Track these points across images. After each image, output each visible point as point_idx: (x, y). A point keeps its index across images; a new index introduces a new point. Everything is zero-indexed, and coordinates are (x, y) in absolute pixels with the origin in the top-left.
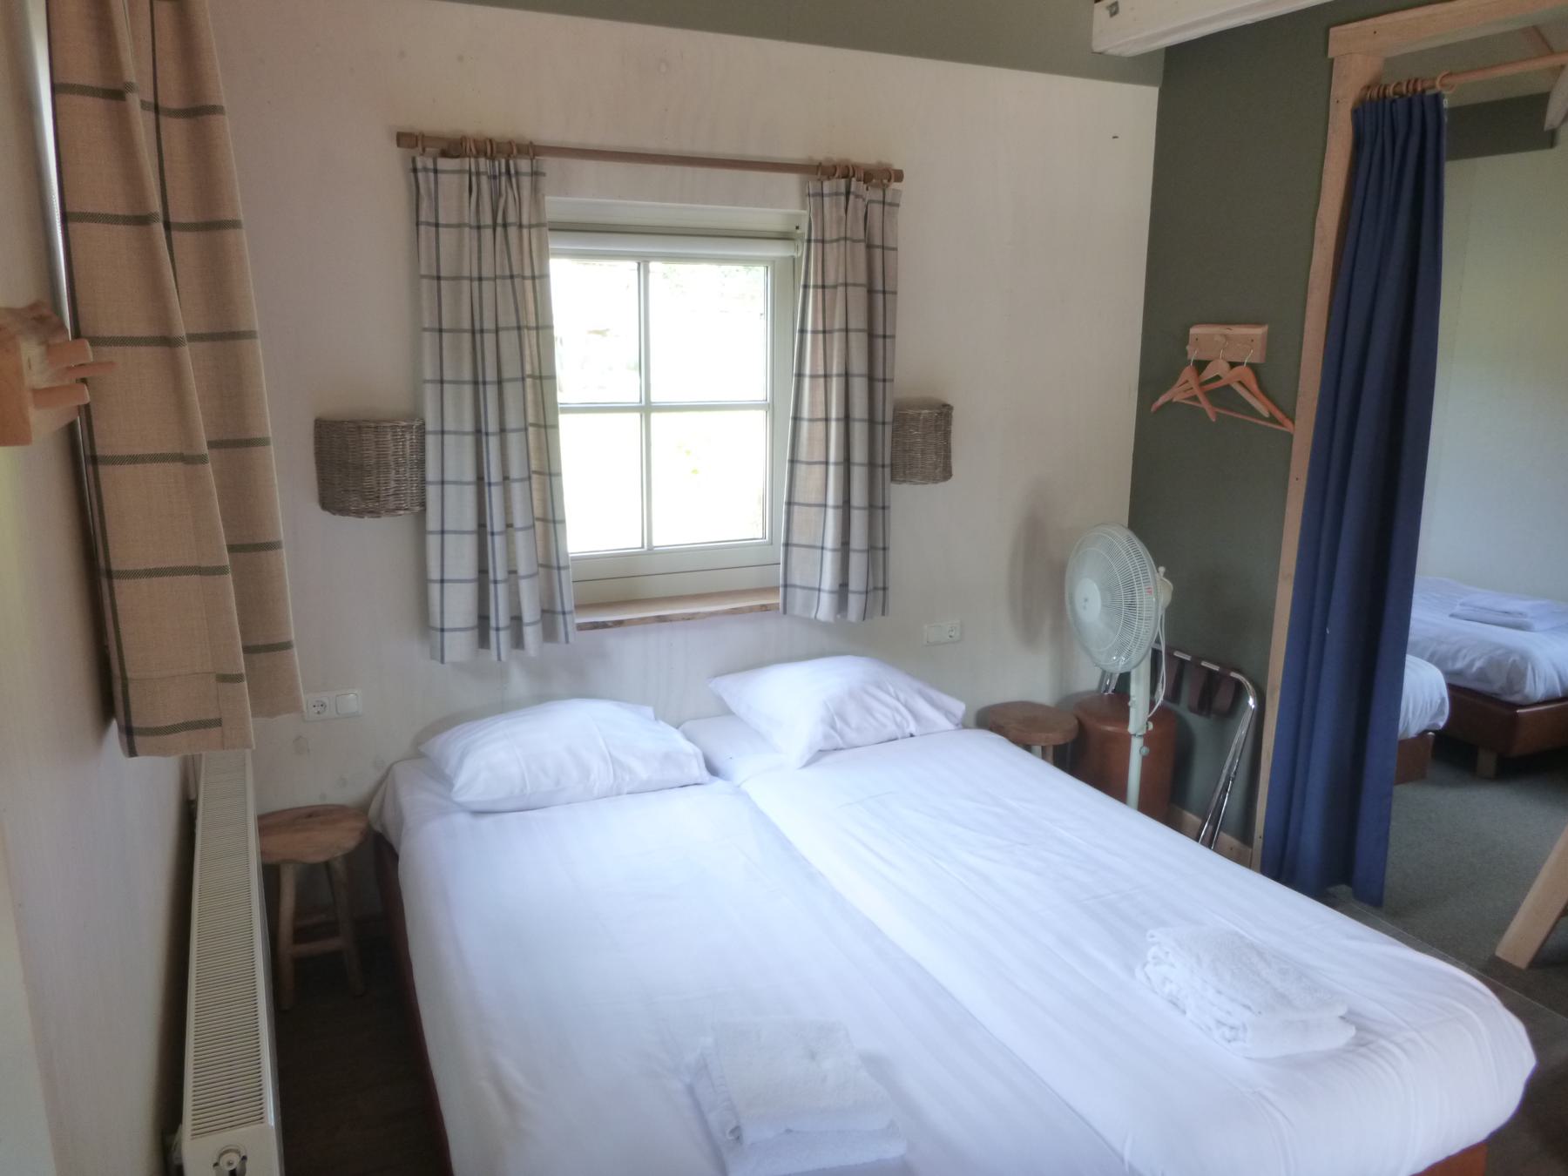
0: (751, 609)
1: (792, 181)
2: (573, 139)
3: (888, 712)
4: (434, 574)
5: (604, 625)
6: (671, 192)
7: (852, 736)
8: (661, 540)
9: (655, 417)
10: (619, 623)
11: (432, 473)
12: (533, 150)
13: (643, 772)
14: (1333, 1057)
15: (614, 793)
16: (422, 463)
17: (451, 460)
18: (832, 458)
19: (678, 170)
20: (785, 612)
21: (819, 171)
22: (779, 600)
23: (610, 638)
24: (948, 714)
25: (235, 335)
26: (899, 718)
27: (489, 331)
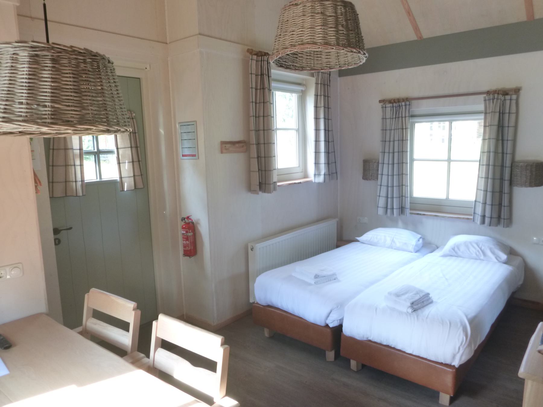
0: (464, 218)
1: (482, 97)
2: (421, 95)
3: (474, 250)
4: (51, 147)
5: (420, 214)
6: (447, 104)
7: (460, 254)
8: (451, 197)
9: (446, 163)
10: (424, 215)
11: (380, 172)
12: (407, 100)
13: (398, 245)
14: (401, 313)
15: (391, 247)
16: (378, 170)
17: (385, 170)
18: (490, 177)
19: (451, 98)
20: (474, 221)
21: (488, 93)
22: (472, 217)
23: (424, 219)
24: (497, 257)
25: (383, 141)
26: (478, 253)
27: (89, 153)
